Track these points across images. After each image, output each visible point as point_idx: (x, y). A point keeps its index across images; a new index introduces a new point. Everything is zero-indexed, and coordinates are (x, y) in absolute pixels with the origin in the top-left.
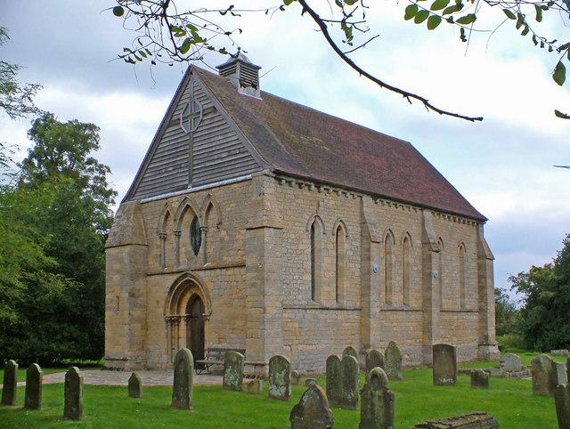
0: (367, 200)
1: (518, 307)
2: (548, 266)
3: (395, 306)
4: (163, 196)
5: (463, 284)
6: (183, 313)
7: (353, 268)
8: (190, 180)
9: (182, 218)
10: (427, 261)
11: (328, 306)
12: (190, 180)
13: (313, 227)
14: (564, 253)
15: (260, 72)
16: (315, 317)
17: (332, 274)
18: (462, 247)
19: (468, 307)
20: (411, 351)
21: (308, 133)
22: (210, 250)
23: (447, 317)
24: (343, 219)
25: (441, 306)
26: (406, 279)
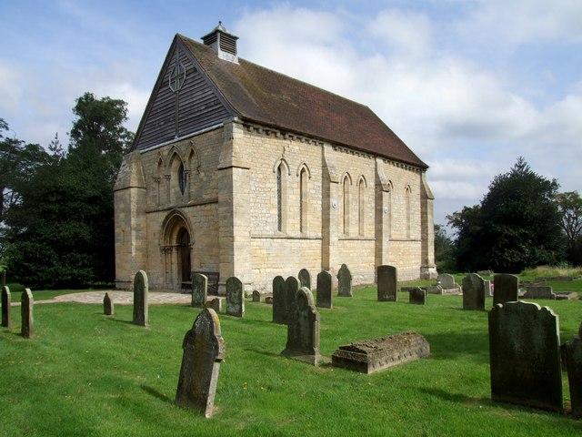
0: (328, 148)
1: (453, 239)
2: (476, 207)
3: (352, 236)
4: (157, 146)
5: (408, 219)
6: (174, 243)
7: (316, 204)
8: (177, 131)
9: (171, 163)
10: (379, 199)
11: (292, 236)
12: (177, 131)
13: (279, 169)
14: (489, 195)
15: (238, 41)
16: (281, 245)
17: (297, 210)
18: (408, 189)
19: (412, 237)
20: (364, 273)
21: (279, 92)
22: (193, 190)
23: (396, 244)
24: (307, 163)
25: (390, 236)
26: (361, 213)
